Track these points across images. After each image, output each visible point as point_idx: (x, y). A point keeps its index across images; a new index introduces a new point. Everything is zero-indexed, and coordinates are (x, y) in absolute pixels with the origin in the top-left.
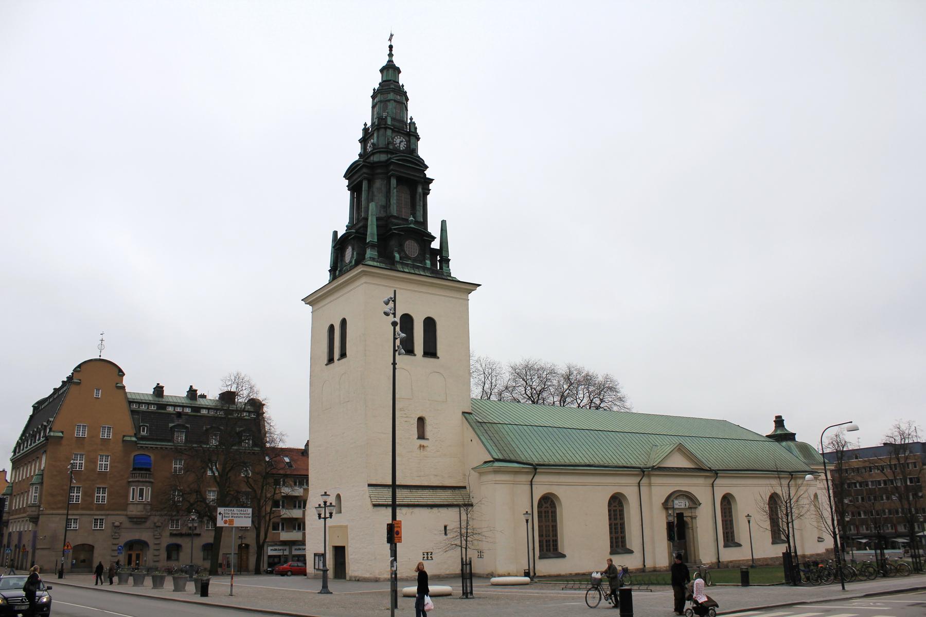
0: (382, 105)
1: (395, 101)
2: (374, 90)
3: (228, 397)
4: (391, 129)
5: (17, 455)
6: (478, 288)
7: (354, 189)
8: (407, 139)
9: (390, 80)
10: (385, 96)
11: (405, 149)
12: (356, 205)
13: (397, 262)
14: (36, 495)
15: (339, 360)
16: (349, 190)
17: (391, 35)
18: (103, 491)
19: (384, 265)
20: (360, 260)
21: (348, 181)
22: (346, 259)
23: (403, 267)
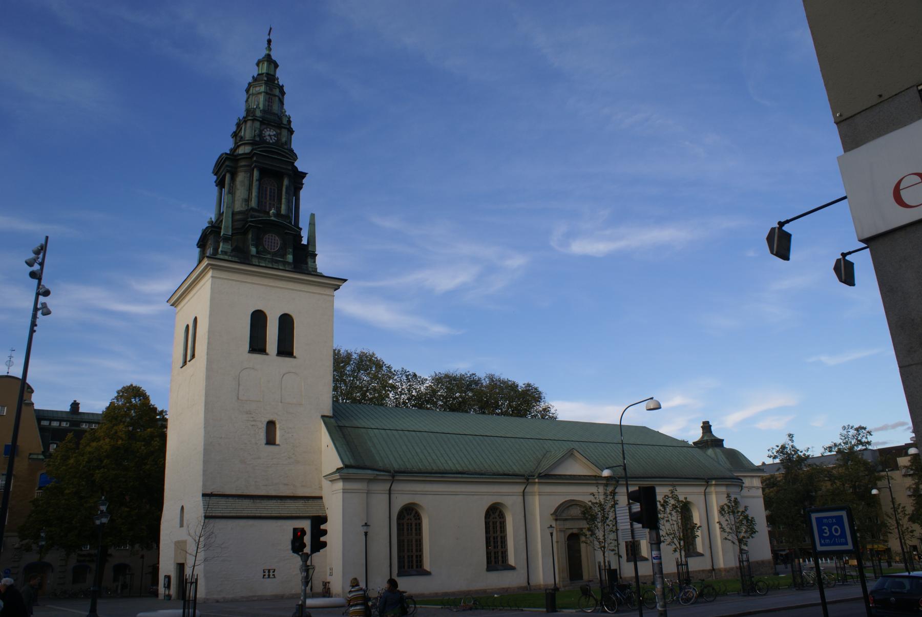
13: (253, 256)
19: (236, 258)
23: (260, 261)
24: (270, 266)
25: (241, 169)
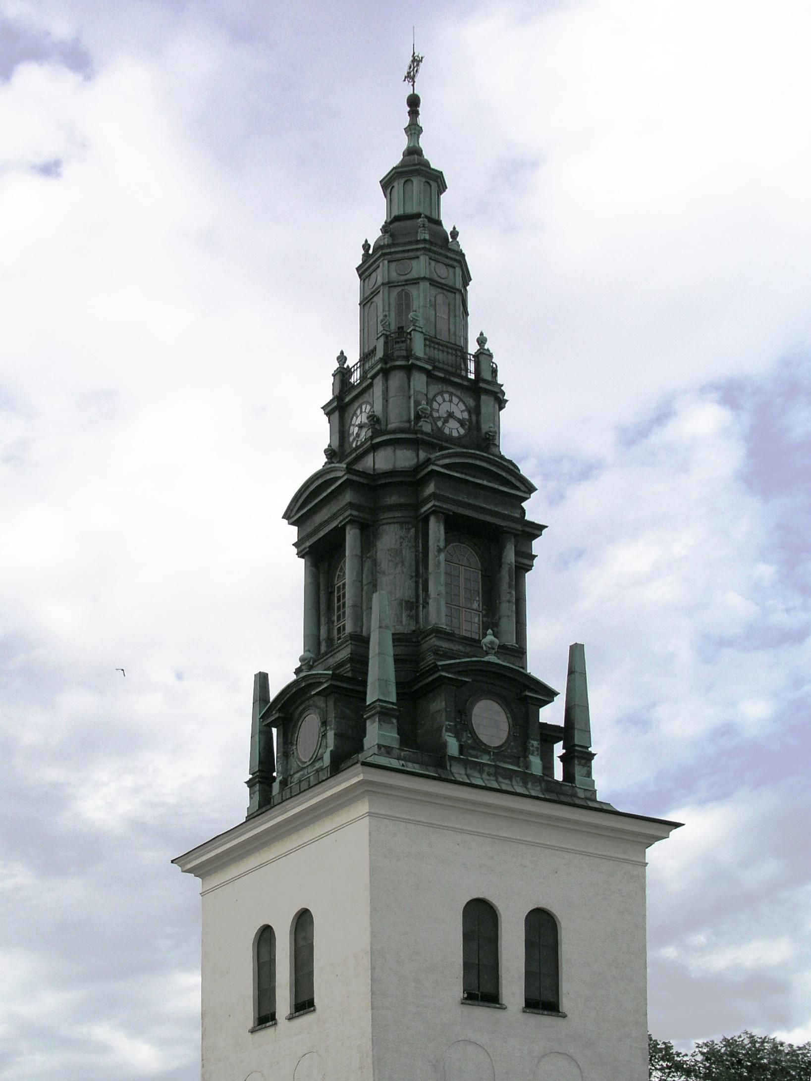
1: (433, 283)
2: (366, 246)
4: (422, 369)
6: (674, 833)
8: (471, 402)
9: (418, 216)
11: (465, 435)
13: (452, 758)
15: (291, 1018)
16: (301, 555)
17: (414, 60)
19: (416, 766)
21: (296, 528)
23: (469, 772)
24: (495, 785)
25: (391, 515)
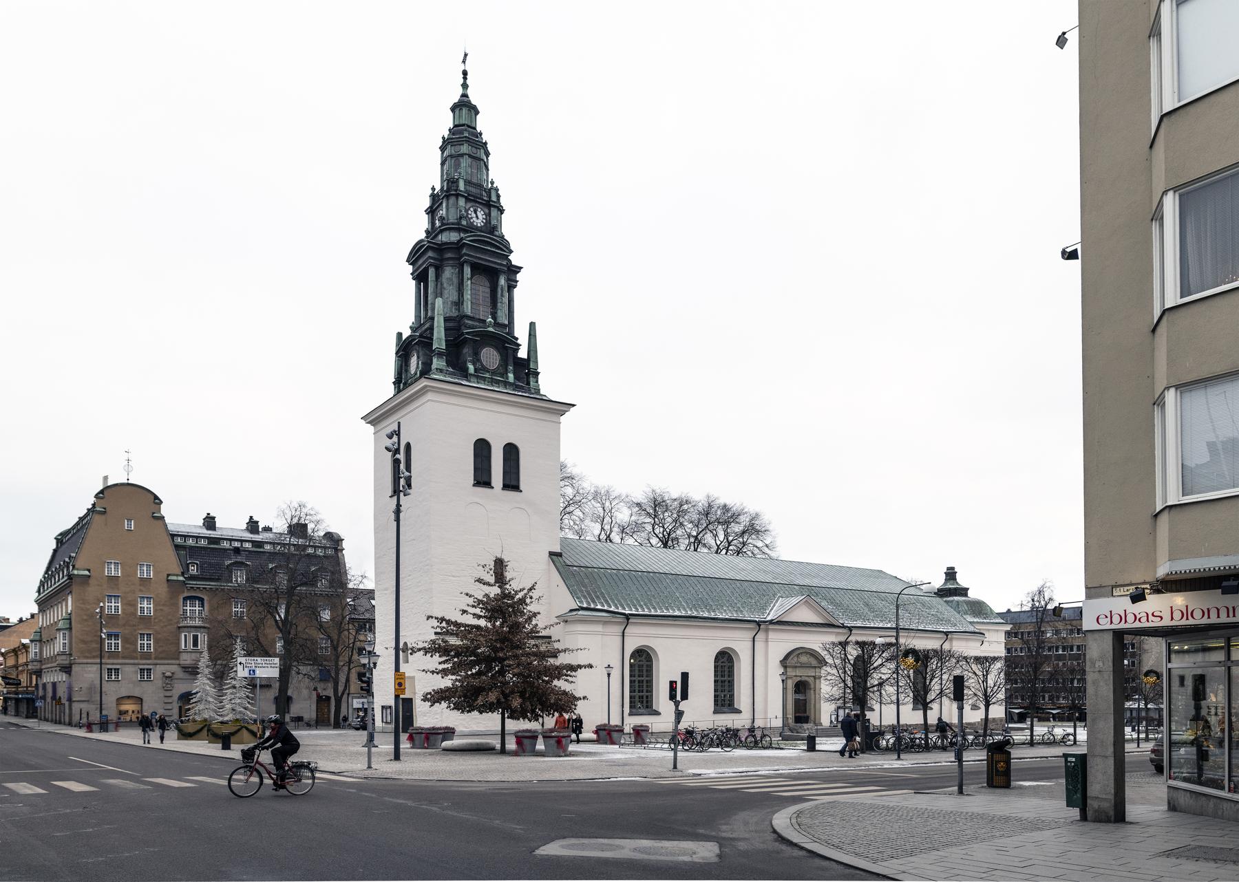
0: (453, 161)
2: (443, 138)
3: (298, 529)
4: (463, 196)
5: (42, 595)
6: (572, 409)
7: (420, 277)
8: (487, 211)
9: (463, 125)
10: (457, 148)
11: (484, 226)
12: (423, 301)
13: (471, 375)
14: (64, 641)
16: (414, 279)
18: (147, 637)
20: (425, 372)
21: (371, 429)
22: (412, 369)
